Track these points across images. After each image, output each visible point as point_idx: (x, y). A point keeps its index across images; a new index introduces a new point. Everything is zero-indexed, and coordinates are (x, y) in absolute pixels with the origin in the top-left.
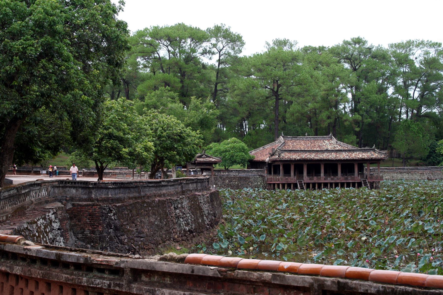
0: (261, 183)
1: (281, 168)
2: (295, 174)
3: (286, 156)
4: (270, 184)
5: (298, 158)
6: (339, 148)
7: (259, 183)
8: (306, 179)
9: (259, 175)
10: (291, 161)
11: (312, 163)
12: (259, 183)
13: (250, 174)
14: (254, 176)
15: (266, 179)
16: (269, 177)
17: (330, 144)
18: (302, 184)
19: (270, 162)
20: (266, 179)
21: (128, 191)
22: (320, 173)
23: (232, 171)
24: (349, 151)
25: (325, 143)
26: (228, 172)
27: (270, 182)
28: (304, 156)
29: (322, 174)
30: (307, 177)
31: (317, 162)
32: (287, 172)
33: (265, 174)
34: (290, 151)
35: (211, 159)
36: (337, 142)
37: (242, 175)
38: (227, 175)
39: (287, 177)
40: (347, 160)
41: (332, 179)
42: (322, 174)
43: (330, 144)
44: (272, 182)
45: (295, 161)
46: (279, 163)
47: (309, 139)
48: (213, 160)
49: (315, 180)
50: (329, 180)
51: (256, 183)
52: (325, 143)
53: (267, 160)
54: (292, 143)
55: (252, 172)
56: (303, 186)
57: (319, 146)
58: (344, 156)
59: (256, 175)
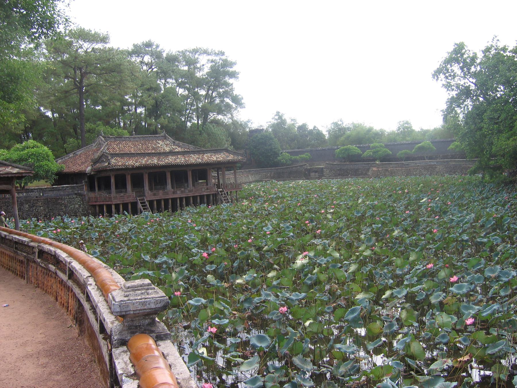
0: (80, 206)
1: (113, 180)
2: (172, 184)
3: (117, 162)
4: (94, 206)
5: (137, 164)
6: (179, 149)
7: (77, 206)
8: (149, 195)
9: (76, 194)
10: (127, 169)
11: (156, 170)
12: (77, 206)
13: (62, 193)
14: (68, 195)
15: (87, 198)
16: (92, 195)
17: (167, 145)
18: (145, 203)
19: (92, 173)
20: (87, 198)
21: (85, 356)
22: (166, 184)
23: (32, 191)
24: (183, 153)
25: (159, 144)
26: (26, 192)
27: (95, 204)
28: (144, 161)
29: (169, 186)
30: (150, 192)
31: (161, 170)
32: (121, 185)
33: (85, 191)
34: (149, 154)
35: (9, 170)
36: (174, 142)
37: (51, 194)
38: (26, 197)
39: (122, 194)
40: (200, 164)
41: (182, 192)
42: (169, 186)
43: (167, 145)
44: (104, 203)
45: (133, 168)
46: (108, 174)
47: (138, 139)
48: (15, 171)
49: (161, 195)
50: (179, 194)
51: (73, 206)
52: (159, 144)
53: (89, 169)
54: (117, 145)
55: (64, 189)
56: (142, 206)
57: (154, 148)
58: (181, 160)
59: (71, 194)
